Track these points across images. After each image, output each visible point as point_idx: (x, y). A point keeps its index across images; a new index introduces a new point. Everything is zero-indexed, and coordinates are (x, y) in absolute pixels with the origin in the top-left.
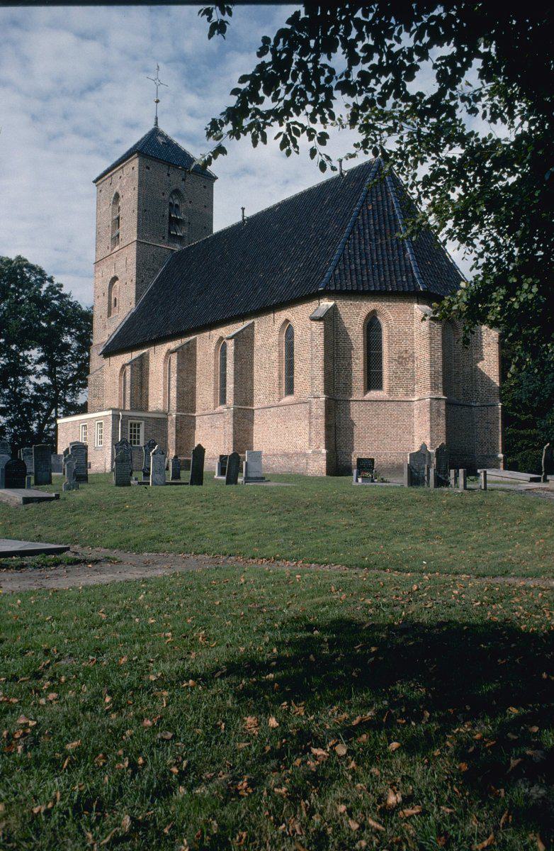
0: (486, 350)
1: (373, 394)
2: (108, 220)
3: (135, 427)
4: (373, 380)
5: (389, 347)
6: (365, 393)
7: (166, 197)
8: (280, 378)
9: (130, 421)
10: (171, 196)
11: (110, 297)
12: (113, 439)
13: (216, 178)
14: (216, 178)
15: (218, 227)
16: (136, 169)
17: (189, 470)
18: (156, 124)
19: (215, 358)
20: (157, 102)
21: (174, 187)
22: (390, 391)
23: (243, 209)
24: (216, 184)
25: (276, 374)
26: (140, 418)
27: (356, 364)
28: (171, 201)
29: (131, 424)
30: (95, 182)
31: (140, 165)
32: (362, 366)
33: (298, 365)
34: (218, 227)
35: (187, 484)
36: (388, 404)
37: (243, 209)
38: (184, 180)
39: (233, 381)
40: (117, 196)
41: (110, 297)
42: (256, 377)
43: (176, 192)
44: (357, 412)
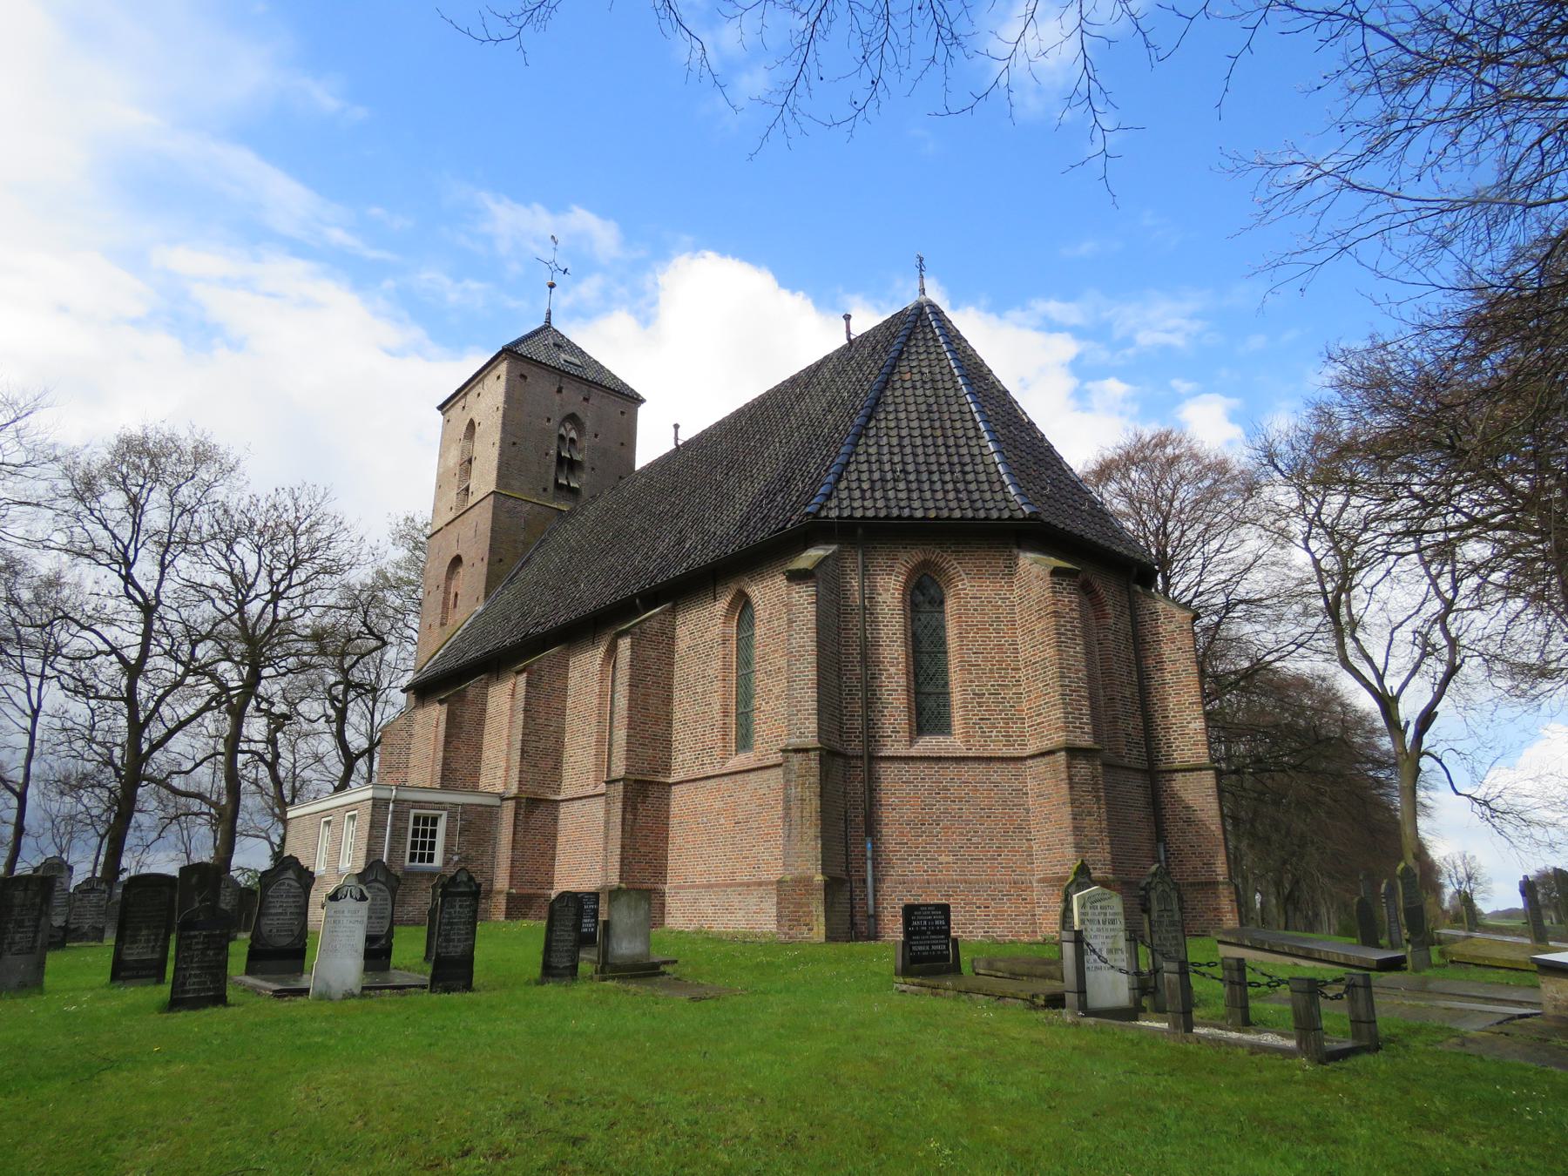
0: (1167, 650)
1: (928, 744)
2: (454, 457)
3: (425, 823)
4: (929, 713)
5: (961, 637)
6: (912, 742)
7: (553, 424)
8: (726, 714)
9: (413, 812)
10: (562, 424)
11: (447, 592)
12: (369, 851)
13: (643, 401)
14: (643, 401)
15: (638, 467)
16: (503, 378)
17: (160, 979)
18: (548, 321)
19: (602, 681)
20: (552, 286)
21: (570, 410)
22: (967, 736)
23: (676, 427)
24: (642, 410)
25: (717, 707)
26: (439, 805)
27: (890, 676)
28: (562, 431)
29: (417, 819)
30: (440, 408)
31: (508, 373)
32: (903, 681)
33: (760, 681)
34: (638, 467)
35: (424, 987)
36: (965, 767)
37: (676, 427)
38: (586, 399)
39: (626, 721)
40: (471, 425)
41: (447, 592)
42: (678, 715)
43: (572, 418)
44: (900, 795)
